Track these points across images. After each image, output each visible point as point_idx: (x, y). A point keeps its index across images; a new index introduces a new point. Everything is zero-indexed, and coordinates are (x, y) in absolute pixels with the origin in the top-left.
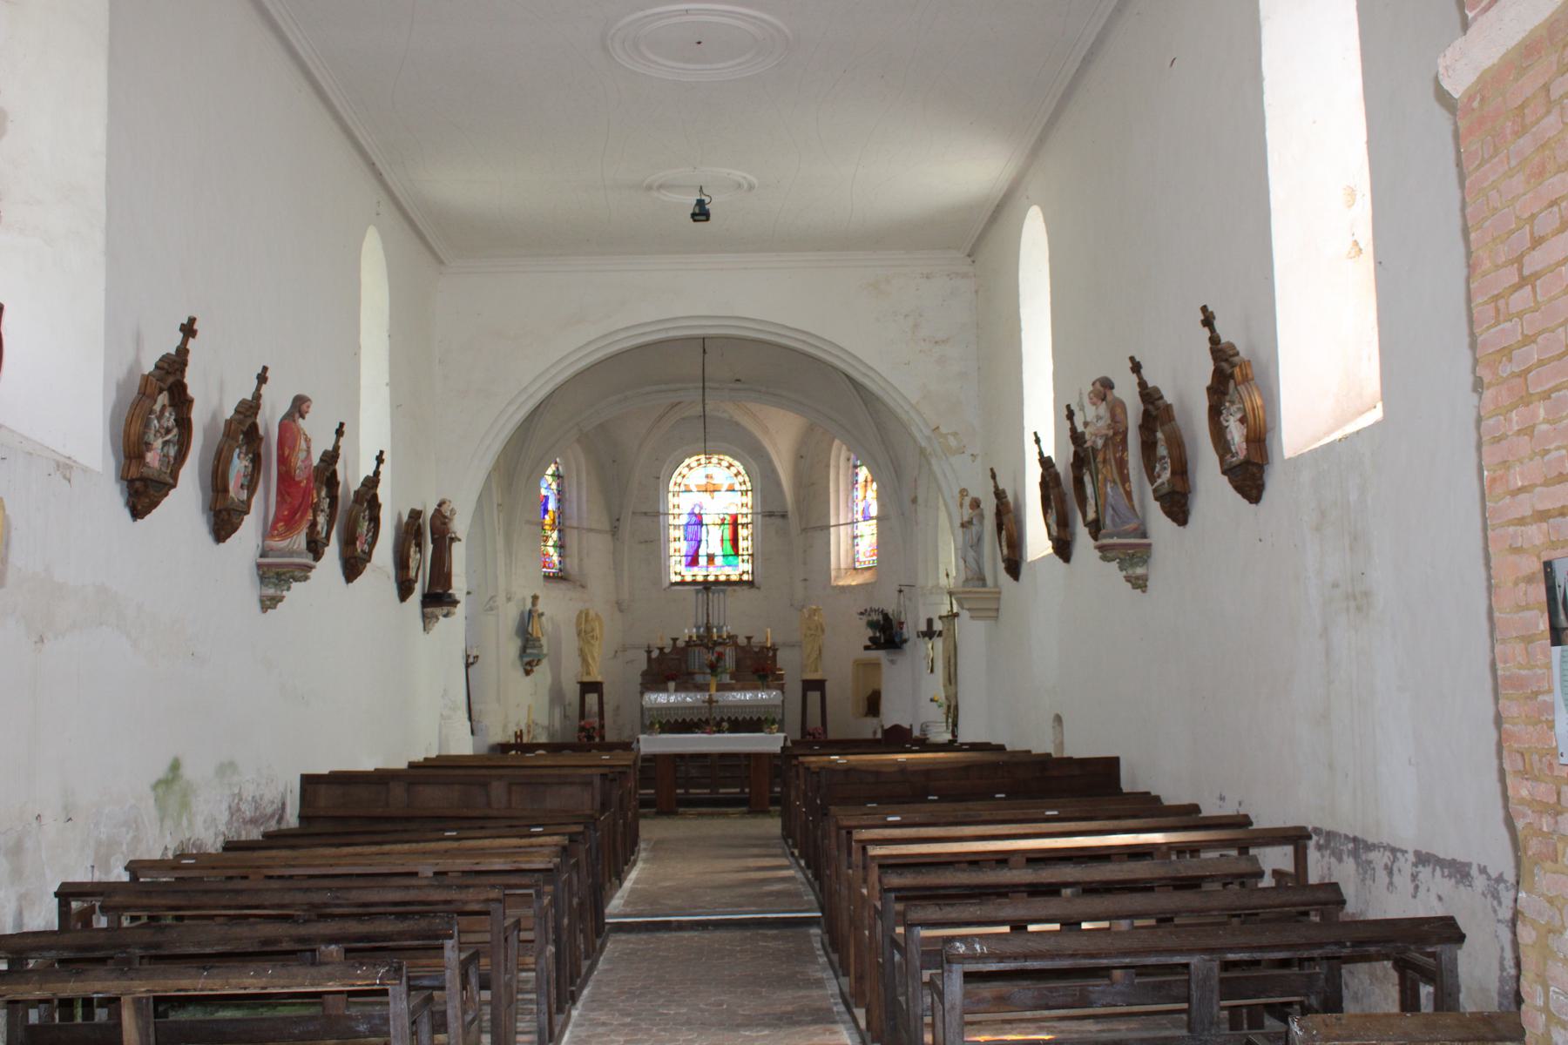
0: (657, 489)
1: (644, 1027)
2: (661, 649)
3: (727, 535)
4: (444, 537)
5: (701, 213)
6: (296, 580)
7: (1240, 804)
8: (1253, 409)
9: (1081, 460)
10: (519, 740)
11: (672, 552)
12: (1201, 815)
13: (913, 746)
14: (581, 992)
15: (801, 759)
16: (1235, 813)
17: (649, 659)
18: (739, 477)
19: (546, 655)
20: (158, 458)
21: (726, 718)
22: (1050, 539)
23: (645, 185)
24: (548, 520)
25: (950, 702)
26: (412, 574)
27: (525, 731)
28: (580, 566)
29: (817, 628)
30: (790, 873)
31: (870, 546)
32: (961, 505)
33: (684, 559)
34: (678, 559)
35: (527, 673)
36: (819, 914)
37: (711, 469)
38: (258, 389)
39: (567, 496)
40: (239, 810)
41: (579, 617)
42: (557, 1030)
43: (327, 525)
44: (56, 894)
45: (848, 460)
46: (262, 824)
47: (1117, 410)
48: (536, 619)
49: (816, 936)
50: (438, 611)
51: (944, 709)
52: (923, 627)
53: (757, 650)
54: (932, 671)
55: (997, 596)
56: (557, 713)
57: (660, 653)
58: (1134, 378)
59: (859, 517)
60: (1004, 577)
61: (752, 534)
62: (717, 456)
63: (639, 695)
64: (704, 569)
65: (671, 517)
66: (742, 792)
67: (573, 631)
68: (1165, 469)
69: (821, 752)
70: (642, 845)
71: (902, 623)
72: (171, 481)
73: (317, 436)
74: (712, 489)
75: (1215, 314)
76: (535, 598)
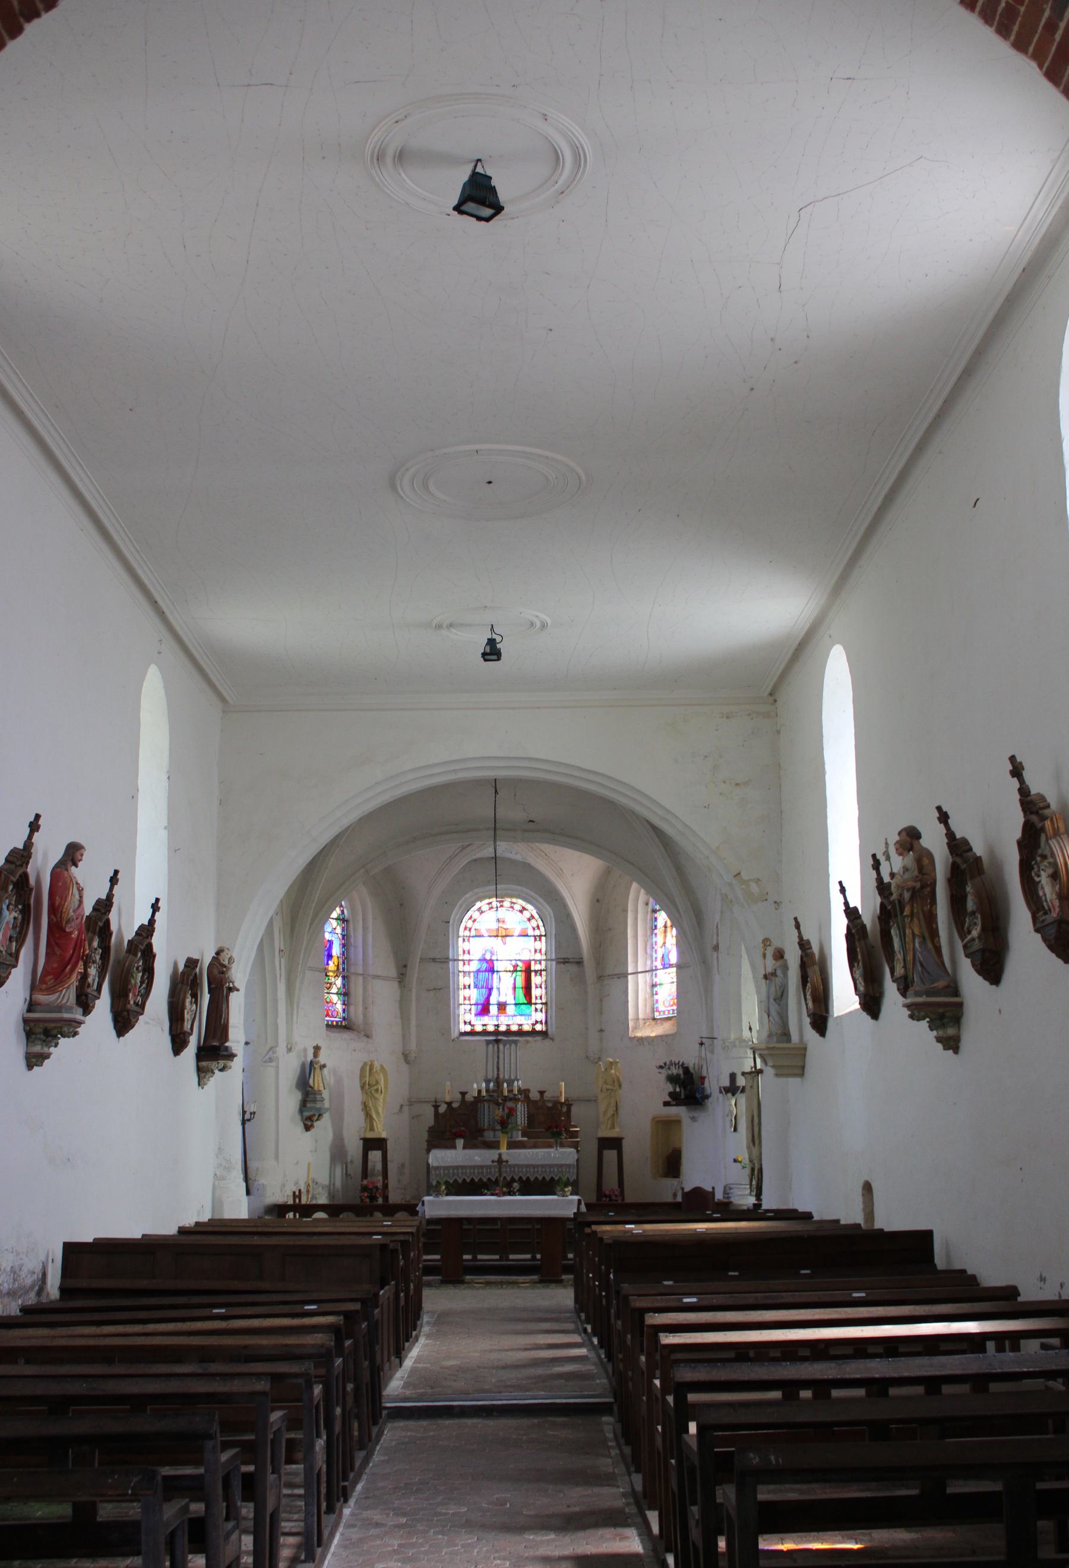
0: (446, 935)
1: (421, 1528)
2: (449, 1104)
3: (520, 982)
4: (222, 986)
5: (492, 652)
6: (64, 1036)
7: (1062, 1286)
9: (886, 915)
10: (297, 1201)
11: (461, 1001)
12: (1020, 1299)
13: (714, 1212)
14: (355, 1487)
15: (594, 1227)
16: (1057, 1298)
17: (436, 1113)
18: (533, 921)
19: (327, 1110)
21: (517, 1178)
22: (856, 994)
23: (434, 623)
24: (332, 966)
25: (754, 1164)
26: (187, 1026)
27: (303, 1190)
28: (365, 1016)
29: (614, 1082)
30: (583, 1351)
31: (669, 995)
32: (764, 956)
33: (473, 1008)
34: (468, 1007)
35: (308, 1128)
36: (612, 1400)
37: (502, 913)
38: (30, 837)
39: (352, 940)
41: (363, 1069)
42: (326, 1533)
43: (99, 978)
45: (647, 904)
46: (20, 1297)
48: (318, 1071)
49: (608, 1424)
50: (213, 1065)
51: (748, 1171)
52: (726, 1083)
53: (550, 1105)
54: (735, 1130)
55: (802, 1051)
56: (339, 1171)
57: (448, 1107)
59: (658, 964)
60: (811, 1034)
61: (546, 981)
62: (509, 900)
63: (425, 1152)
64: (495, 1018)
65: (461, 963)
66: (534, 1258)
67: (357, 1085)
68: (975, 924)
69: (617, 1219)
70: (425, 1318)
74: (504, 934)
75: (1024, 764)
76: (317, 1049)
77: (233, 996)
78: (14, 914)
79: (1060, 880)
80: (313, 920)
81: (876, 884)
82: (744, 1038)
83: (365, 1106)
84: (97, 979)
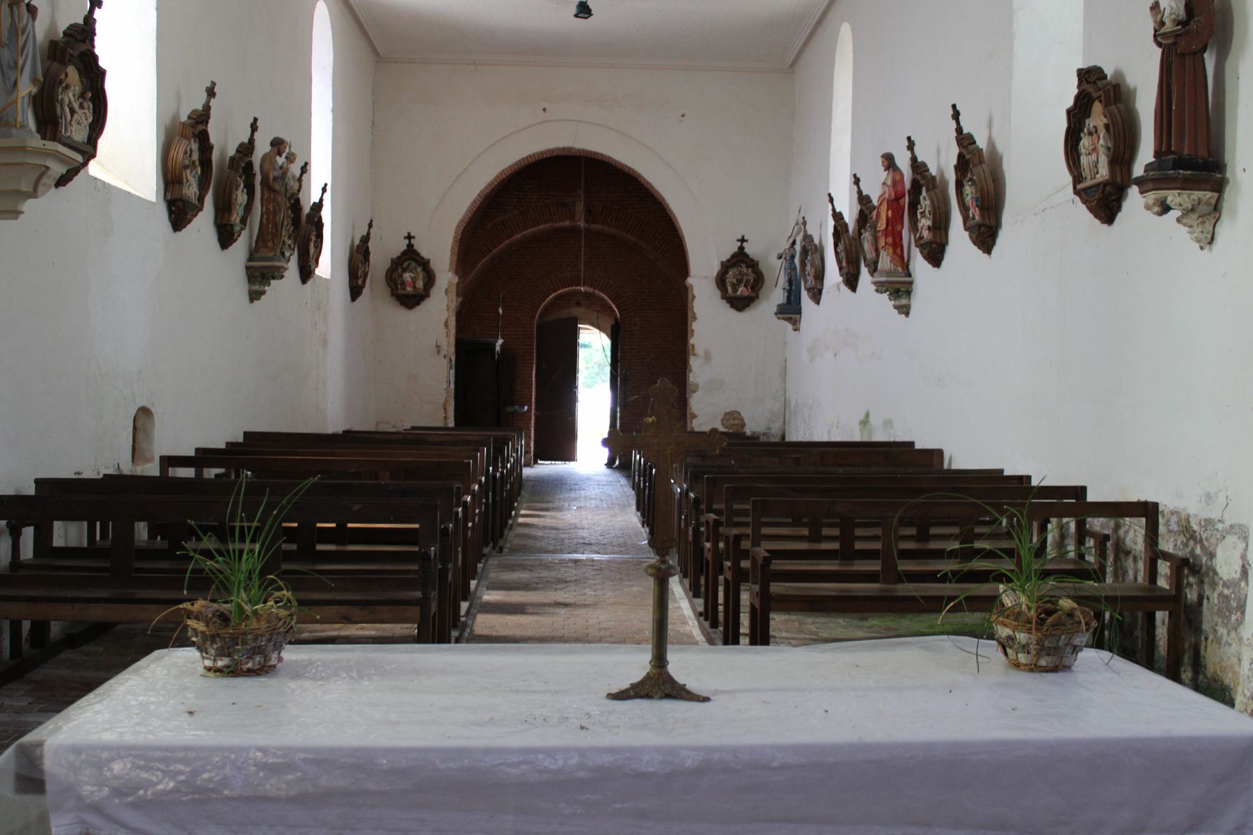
58: (909, 154)
72: (199, 205)
81: (910, 163)
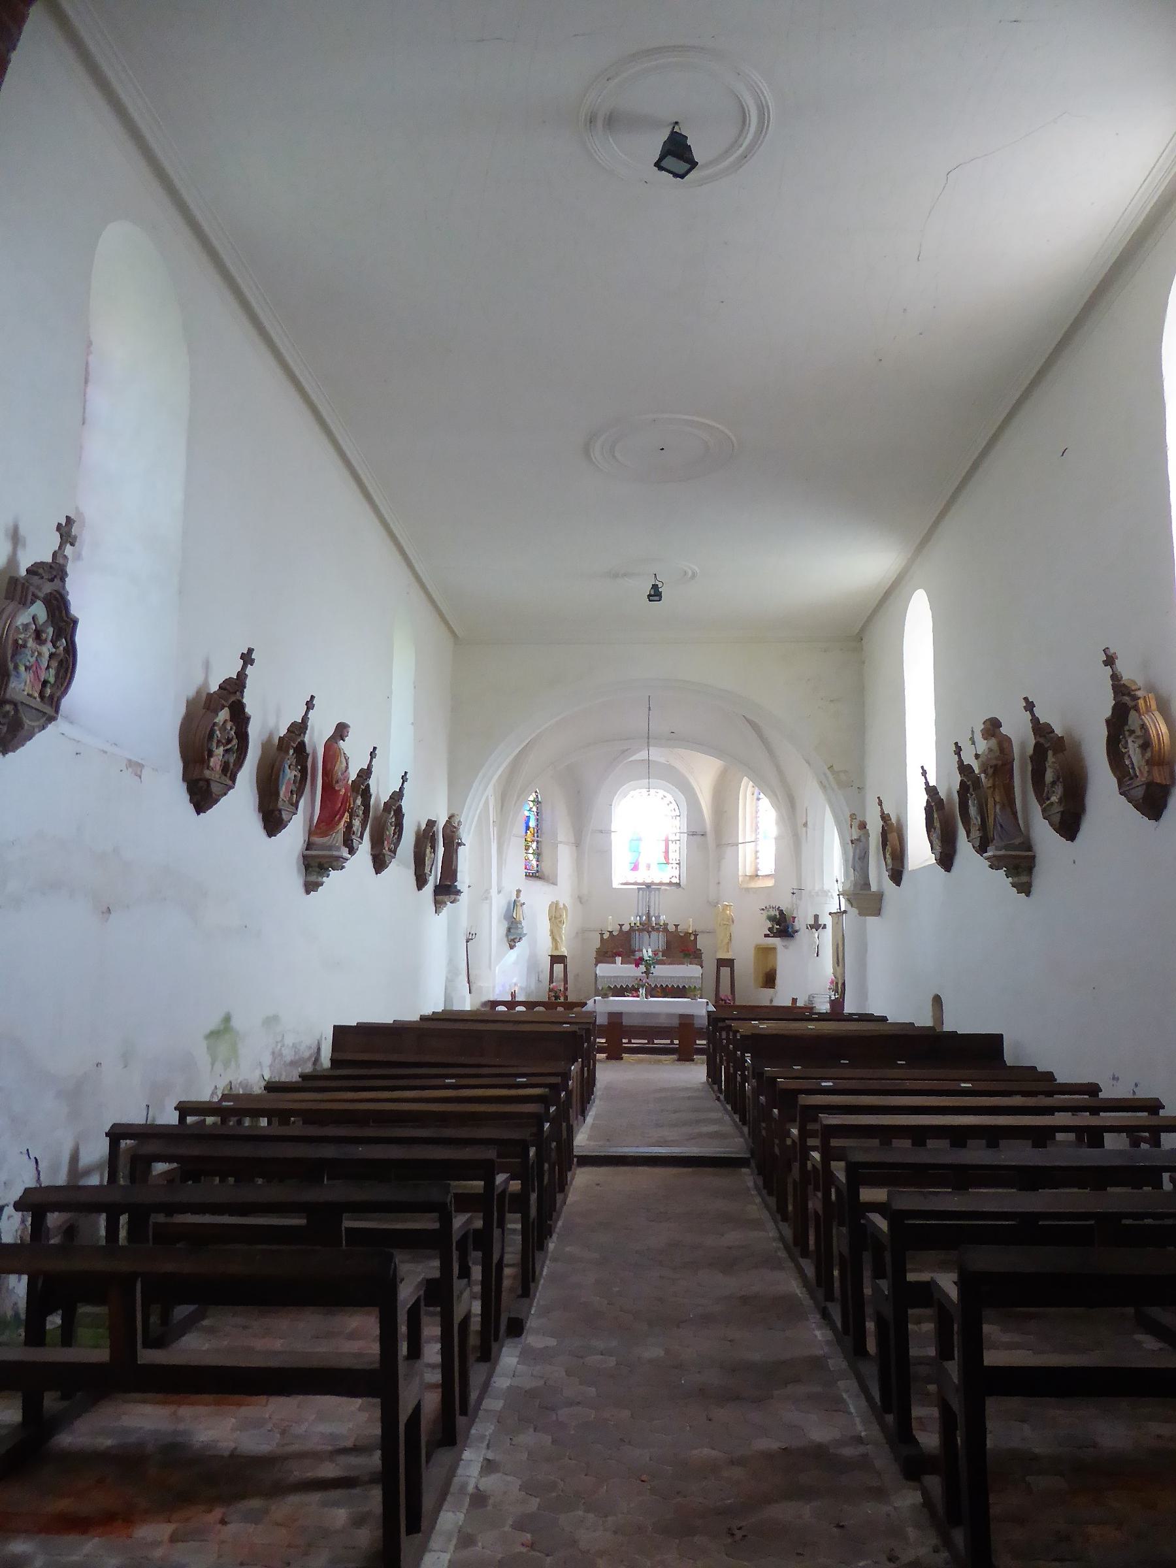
5: (655, 594)
7: (1136, 1085)
8: (1158, 735)
17: (602, 939)
19: (526, 934)
20: (220, 763)
26: (427, 870)
30: (714, 1115)
40: (281, 1055)
44: (107, 1135)
45: (753, 794)
47: (1004, 744)
50: (445, 898)
53: (682, 935)
55: (879, 897)
60: (888, 884)
66: (672, 1043)
71: (794, 918)
73: (355, 757)
76: (519, 891)
77: (461, 849)
78: (294, 773)
79: (1152, 749)
80: (516, 802)
82: (825, 889)
83: (552, 932)
84: (360, 829)
